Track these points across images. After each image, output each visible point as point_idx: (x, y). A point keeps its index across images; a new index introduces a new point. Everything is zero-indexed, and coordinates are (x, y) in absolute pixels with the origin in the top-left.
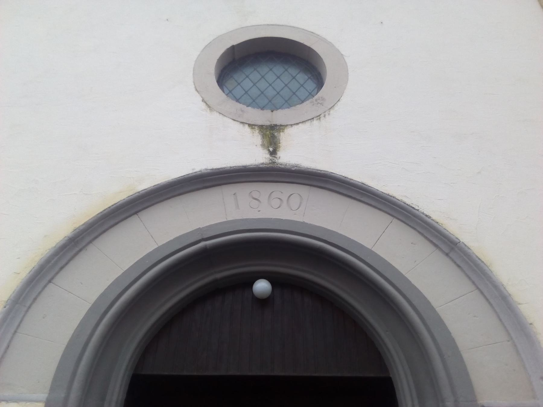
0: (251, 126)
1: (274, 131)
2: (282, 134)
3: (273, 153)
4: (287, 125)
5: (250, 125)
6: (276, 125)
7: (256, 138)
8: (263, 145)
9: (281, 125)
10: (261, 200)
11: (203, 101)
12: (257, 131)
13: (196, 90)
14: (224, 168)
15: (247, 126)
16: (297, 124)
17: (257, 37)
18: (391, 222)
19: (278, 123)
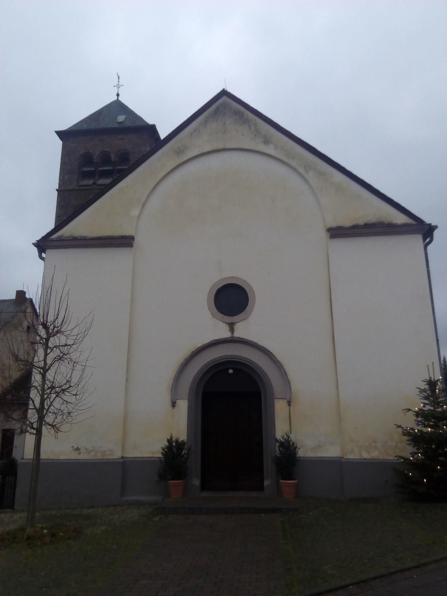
0: (226, 323)
1: (408, 431)
2: (235, 326)
3: (232, 333)
4: (236, 323)
5: (225, 323)
6: (233, 323)
7: (226, 328)
8: (229, 330)
9: (235, 323)
10: (415, 421)
11: (211, 314)
12: (228, 325)
13: (209, 309)
14: (220, 339)
15: (225, 323)
16: (239, 322)
17: (106, 194)
18: (82, 365)
19: (234, 322)
